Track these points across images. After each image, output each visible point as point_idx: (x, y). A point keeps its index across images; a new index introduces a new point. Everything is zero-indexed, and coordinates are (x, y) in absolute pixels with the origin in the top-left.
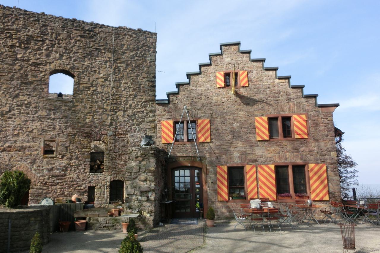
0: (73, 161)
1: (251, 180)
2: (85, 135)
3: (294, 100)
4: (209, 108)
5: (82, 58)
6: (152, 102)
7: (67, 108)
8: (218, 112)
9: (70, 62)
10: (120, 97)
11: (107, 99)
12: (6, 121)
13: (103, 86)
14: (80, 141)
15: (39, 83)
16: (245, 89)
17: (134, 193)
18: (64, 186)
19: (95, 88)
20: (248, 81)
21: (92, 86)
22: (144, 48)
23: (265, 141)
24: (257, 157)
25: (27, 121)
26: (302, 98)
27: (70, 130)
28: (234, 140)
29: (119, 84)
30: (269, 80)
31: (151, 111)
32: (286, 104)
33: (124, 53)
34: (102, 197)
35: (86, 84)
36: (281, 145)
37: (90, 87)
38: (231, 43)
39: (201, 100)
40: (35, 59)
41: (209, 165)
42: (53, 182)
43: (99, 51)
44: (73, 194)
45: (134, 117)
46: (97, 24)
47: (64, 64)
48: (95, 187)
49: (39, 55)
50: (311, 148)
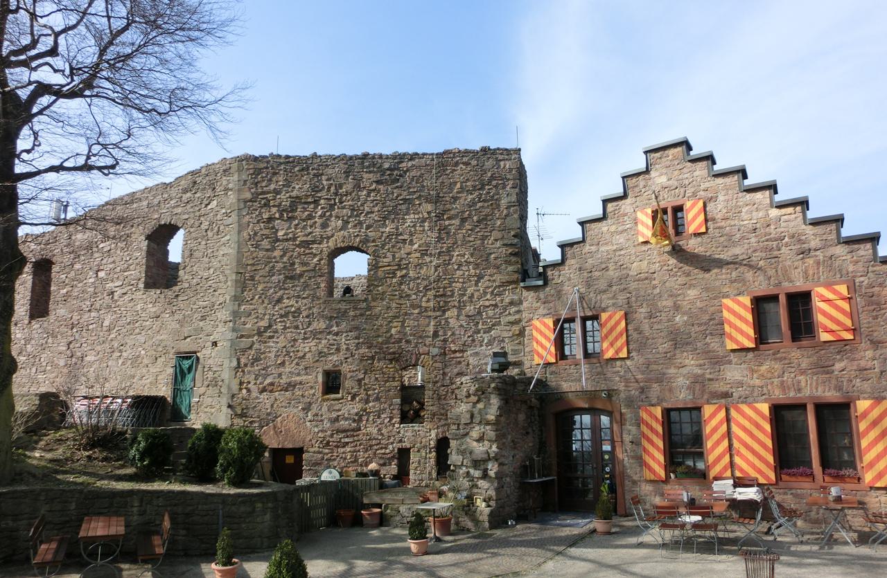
0: (370, 404)
1: (716, 437)
2: (389, 357)
3: (818, 253)
4: (622, 287)
5: (380, 221)
6: (514, 286)
7: (358, 312)
8: (642, 293)
9: (360, 231)
10: (450, 283)
11: (427, 289)
12: (265, 342)
13: (419, 266)
14: (382, 368)
15: (312, 274)
16: (699, 239)
17: (462, 462)
18: (357, 448)
19: (404, 271)
20: (706, 220)
21: (400, 269)
22: (494, 183)
23: (748, 350)
24: (729, 386)
25: (295, 340)
26: (839, 246)
27: (364, 350)
28: (678, 351)
29: (447, 258)
30: (754, 213)
31: (512, 303)
32: (796, 263)
33: (455, 199)
34: (422, 467)
36: (785, 359)
37: (397, 270)
38: (665, 144)
39: (608, 273)
40: (304, 236)
41: (625, 405)
42: (340, 442)
43: (409, 204)
44: (371, 462)
45: (479, 317)
46: (404, 154)
47: (350, 236)
48: (410, 448)
49: (311, 227)
50: (863, 363)
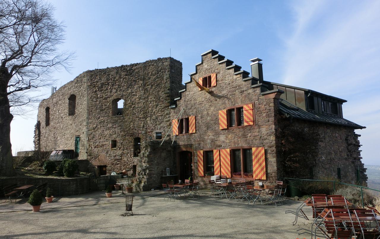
2: (130, 135)
35: (129, 104)
